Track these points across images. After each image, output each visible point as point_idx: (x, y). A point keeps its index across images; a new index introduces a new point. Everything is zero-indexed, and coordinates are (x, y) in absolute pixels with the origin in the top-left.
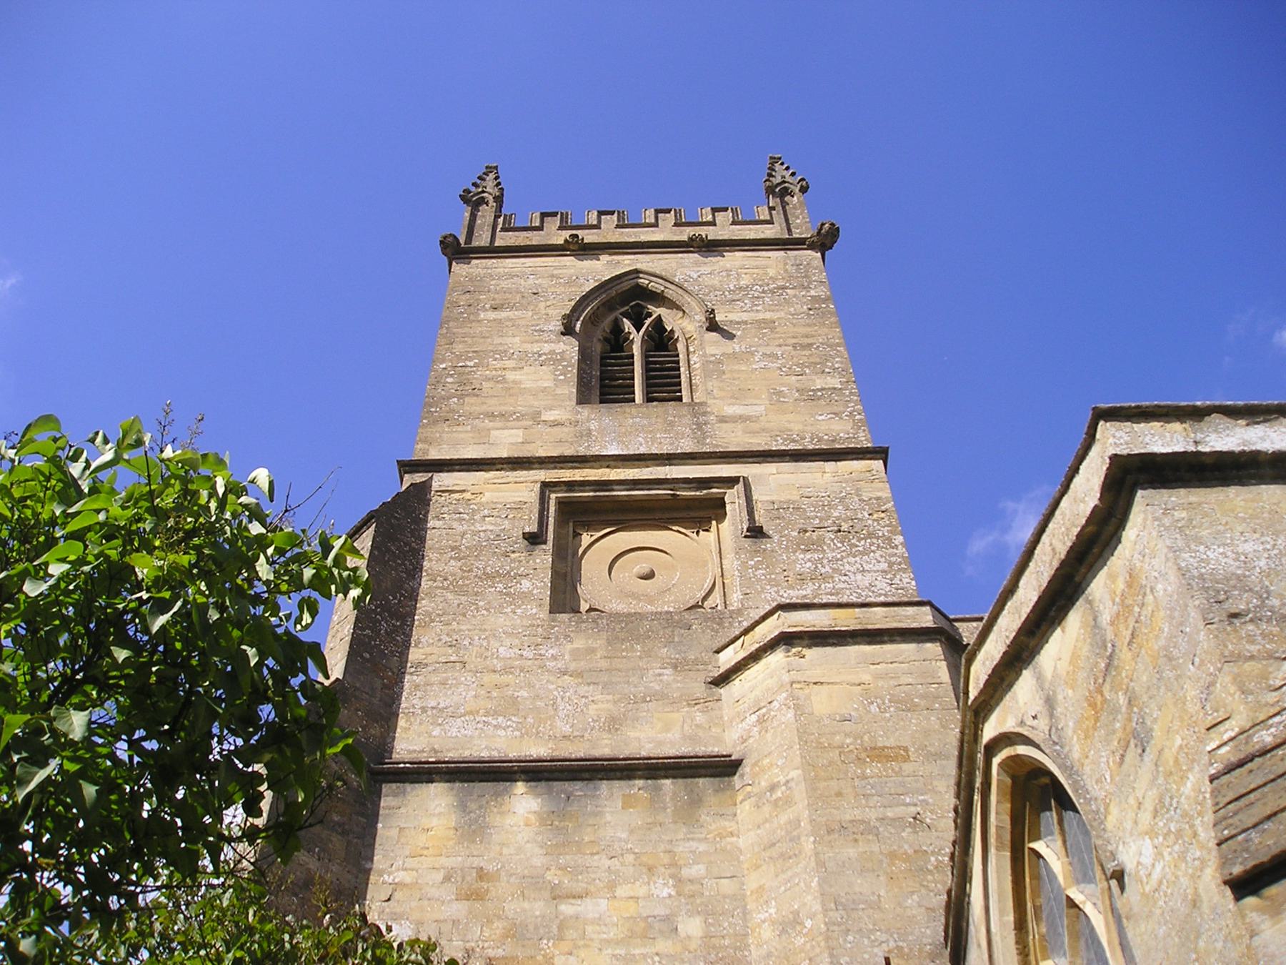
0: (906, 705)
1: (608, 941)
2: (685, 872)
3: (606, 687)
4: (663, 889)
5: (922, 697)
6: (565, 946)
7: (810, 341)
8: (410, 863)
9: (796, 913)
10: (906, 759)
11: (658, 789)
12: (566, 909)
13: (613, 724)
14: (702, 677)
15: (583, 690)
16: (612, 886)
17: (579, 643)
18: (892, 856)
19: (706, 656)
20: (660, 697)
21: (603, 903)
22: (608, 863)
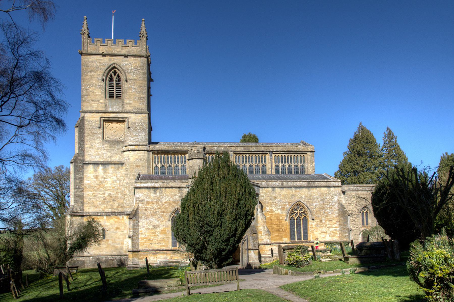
0: (141, 160)
12: (106, 180)
13: (110, 157)
17: (106, 145)
20: (116, 153)
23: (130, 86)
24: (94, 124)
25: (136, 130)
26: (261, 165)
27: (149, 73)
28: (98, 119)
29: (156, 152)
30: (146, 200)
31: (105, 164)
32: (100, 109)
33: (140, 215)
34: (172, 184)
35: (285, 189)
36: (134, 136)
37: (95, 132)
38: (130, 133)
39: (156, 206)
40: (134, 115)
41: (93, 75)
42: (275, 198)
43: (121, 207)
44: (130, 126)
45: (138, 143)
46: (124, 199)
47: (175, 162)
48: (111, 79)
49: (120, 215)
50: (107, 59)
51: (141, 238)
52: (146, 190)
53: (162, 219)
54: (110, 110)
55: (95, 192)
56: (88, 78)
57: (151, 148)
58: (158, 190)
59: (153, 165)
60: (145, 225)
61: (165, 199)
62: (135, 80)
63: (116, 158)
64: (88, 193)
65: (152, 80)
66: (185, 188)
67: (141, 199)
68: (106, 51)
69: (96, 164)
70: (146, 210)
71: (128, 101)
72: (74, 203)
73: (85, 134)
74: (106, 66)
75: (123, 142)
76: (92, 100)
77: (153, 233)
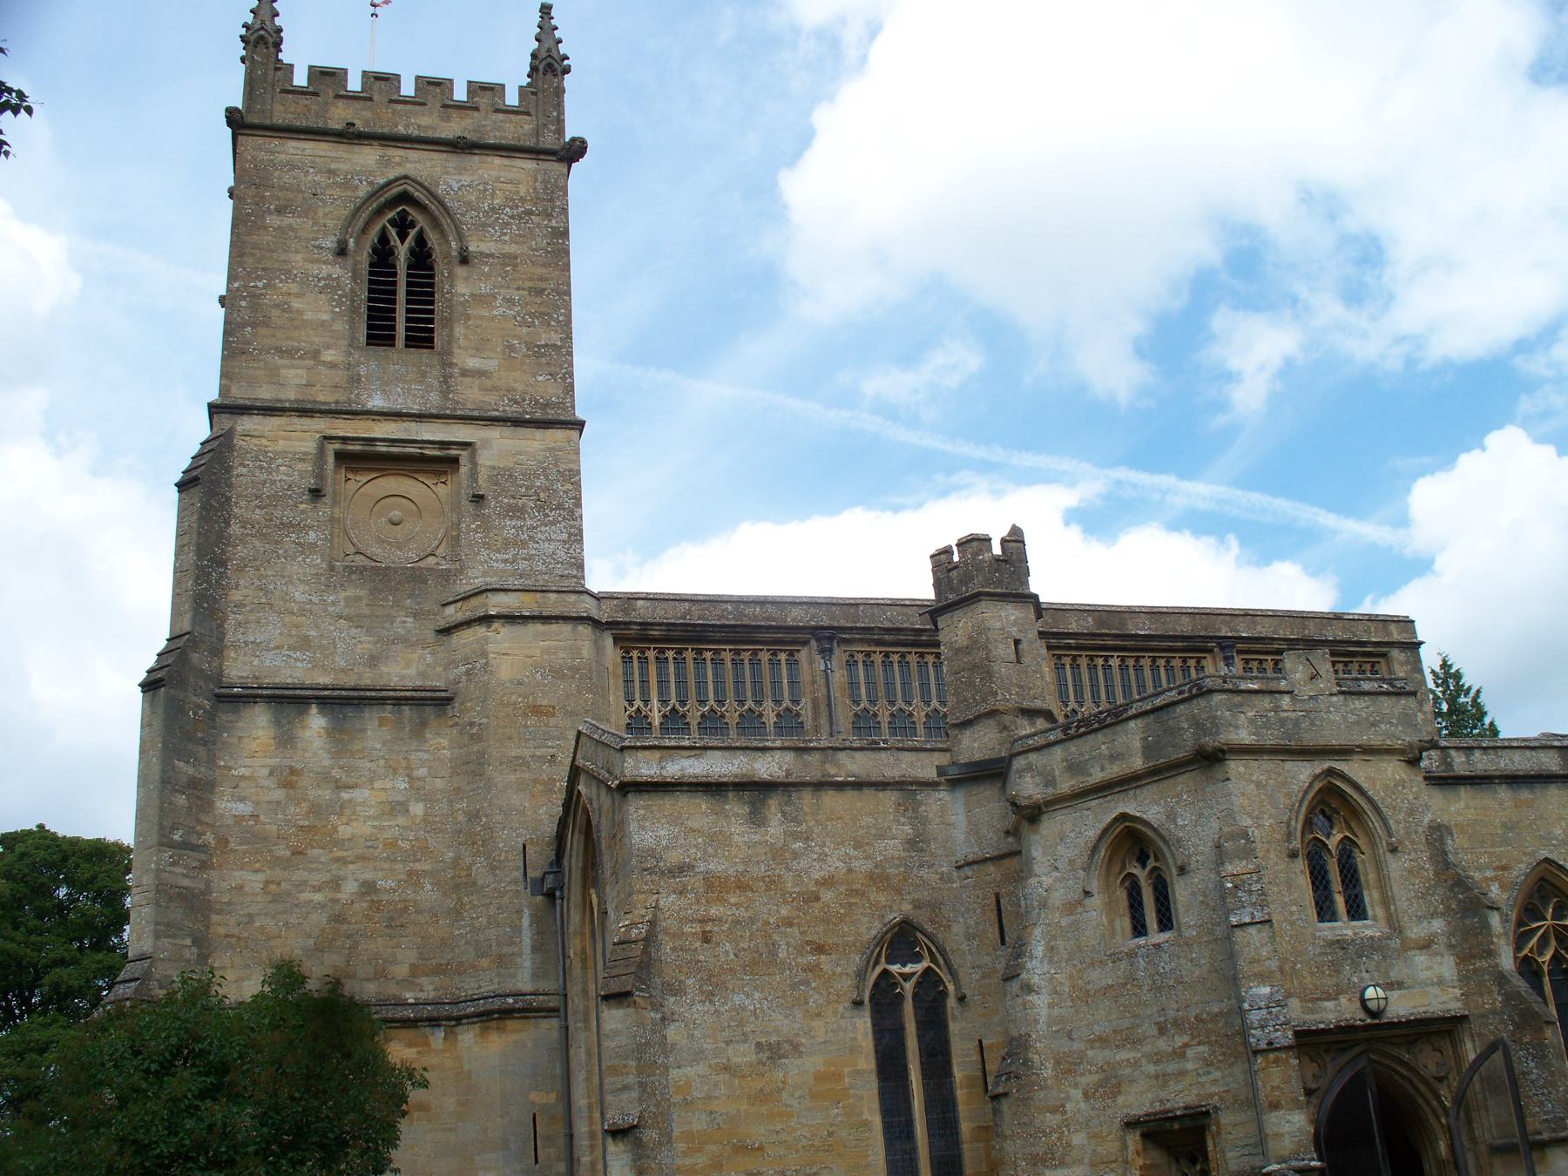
0: (558, 673)
1: (369, 817)
2: (415, 773)
3: (369, 632)
4: (402, 784)
5: (569, 669)
6: (344, 819)
7: (542, 285)
8: (248, 762)
9: (478, 811)
10: (553, 715)
11: (400, 713)
12: (345, 795)
13: (373, 661)
14: (433, 627)
15: (354, 631)
16: (371, 781)
17: (350, 592)
18: (536, 781)
19: (436, 608)
20: (405, 640)
21: (367, 792)
22: (369, 765)
23: (484, 288)
24: (282, 475)
25: (516, 512)
28: (309, 445)
30: (701, 867)
31: (344, 703)
32: (321, 398)
33: (669, 974)
35: (1464, 793)
36: (507, 544)
37: (289, 515)
38: (486, 527)
40: (508, 431)
41: (290, 227)
43: (439, 970)
44: (483, 487)
46: (457, 913)
49: (434, 1022)
50: (367, 157)
51: (689, 1136)
52: (702, 804)
53: (815, 999)
54: (377, 402)
55: (278, 873)
56: (266, 238)
58: (774, 804)
60: (708, 1046)
61: (822, 858)
62: (510, 259)
63: (405, 669)
64: (238, 876)
66: (933, 785)
67: (673, 857)
68: (367, 123)
69: (290, 701)
70: (706, 938)
71: (473, 363)
72: (157, 937)
73: (235, 529)
74: (363, 191)
76: (280, 351)
77: (761, 1097)
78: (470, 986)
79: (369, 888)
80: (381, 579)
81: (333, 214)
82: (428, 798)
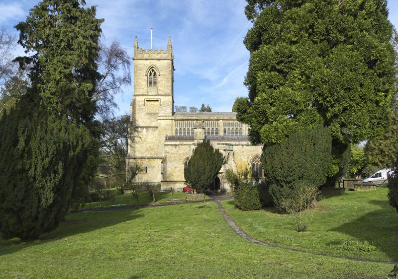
13: (150, 123)
25: (165, 106)
26: (239, 128)
27: (173, 78)
29: (176, 120)
34: (185, 143)
38: (162, 108)
39: (176, 155)
42: (244, 152)
45: (166, 115)
46: (158, 149)
47: (187, 126)
48: (151, 74)
50: (148, 61)
52: (171, 146)
54: (150, 94)
56: (137, 74)
57: (173, 117)
58: (177, 146)
59: (174, 128)
62: (165, 75)
63: (153, 124)
65: (174, 70)
71: (160, 89)
75: (157, 114)
78: (159, 156)
79: (150, 146)
80: (150, 114)
81: (145, 70)
82: (155, 137)
